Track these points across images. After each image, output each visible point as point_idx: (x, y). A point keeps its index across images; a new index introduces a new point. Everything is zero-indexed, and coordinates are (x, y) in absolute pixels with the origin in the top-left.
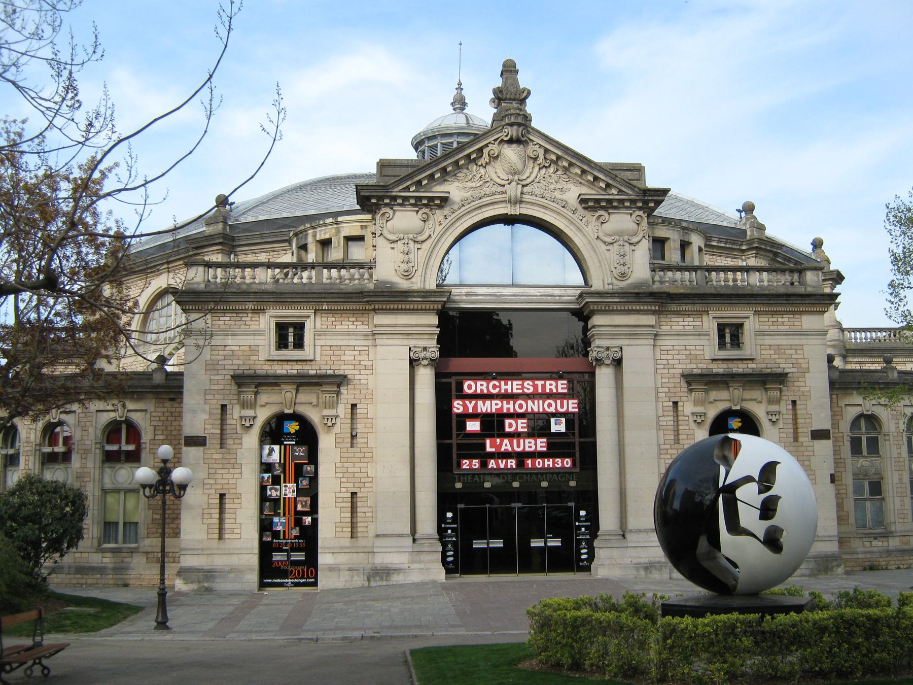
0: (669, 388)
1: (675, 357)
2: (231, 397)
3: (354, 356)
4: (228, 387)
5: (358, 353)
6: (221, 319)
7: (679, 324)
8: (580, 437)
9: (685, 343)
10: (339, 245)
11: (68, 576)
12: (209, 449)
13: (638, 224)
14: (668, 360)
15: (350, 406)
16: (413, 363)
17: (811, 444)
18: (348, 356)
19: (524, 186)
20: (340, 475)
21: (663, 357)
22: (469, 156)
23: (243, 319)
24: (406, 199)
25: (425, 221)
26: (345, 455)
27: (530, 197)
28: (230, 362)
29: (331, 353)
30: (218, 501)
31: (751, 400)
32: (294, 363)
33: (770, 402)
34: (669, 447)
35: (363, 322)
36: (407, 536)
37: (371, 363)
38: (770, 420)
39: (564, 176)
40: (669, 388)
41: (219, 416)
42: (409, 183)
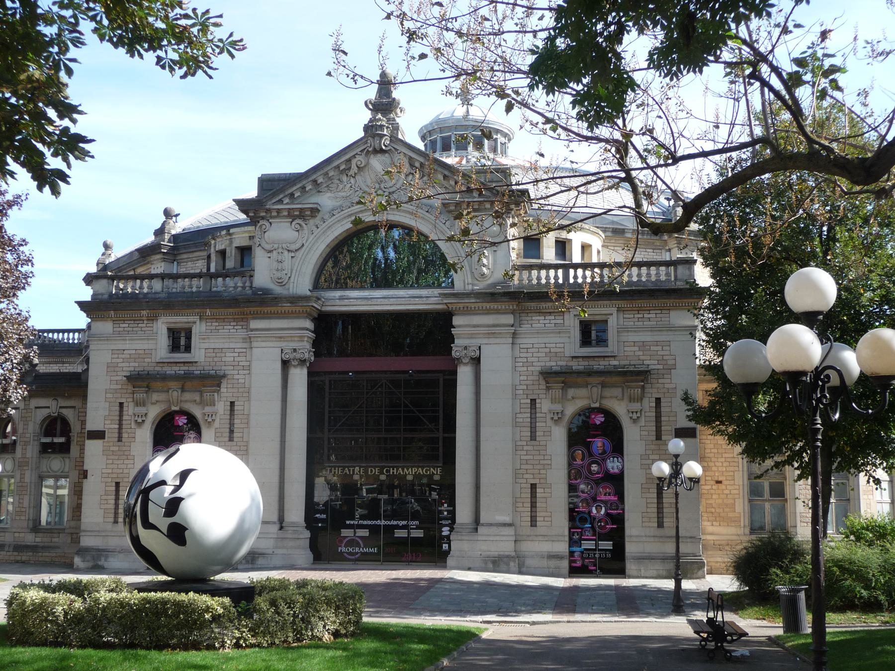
0: (527, 385)
1: (535, 355)
2: (127, 396)
4: (125, 387)
5: (237, 354)
6: (121, 325)
7: (538, 322)
8: (444, 432)
9: (546, 340)
10: (231, 255)
11: (8, 553)
12: (108, 442)
14: (527, 358)
15: (229, 404)
18: (229, 358)
21: (522, 355)
22: (338, 167)
23: (140, 325)
24: (279, 211)
28: (127, 364)
29: (214, 355)
30: (114, 488)
31: (611, 397)
33: (631, 399)
36: (274, 523)
37: (248, 364)
38: (631, 418)
40: (527, 385)
41: (118, 413)
42: (281, 196)
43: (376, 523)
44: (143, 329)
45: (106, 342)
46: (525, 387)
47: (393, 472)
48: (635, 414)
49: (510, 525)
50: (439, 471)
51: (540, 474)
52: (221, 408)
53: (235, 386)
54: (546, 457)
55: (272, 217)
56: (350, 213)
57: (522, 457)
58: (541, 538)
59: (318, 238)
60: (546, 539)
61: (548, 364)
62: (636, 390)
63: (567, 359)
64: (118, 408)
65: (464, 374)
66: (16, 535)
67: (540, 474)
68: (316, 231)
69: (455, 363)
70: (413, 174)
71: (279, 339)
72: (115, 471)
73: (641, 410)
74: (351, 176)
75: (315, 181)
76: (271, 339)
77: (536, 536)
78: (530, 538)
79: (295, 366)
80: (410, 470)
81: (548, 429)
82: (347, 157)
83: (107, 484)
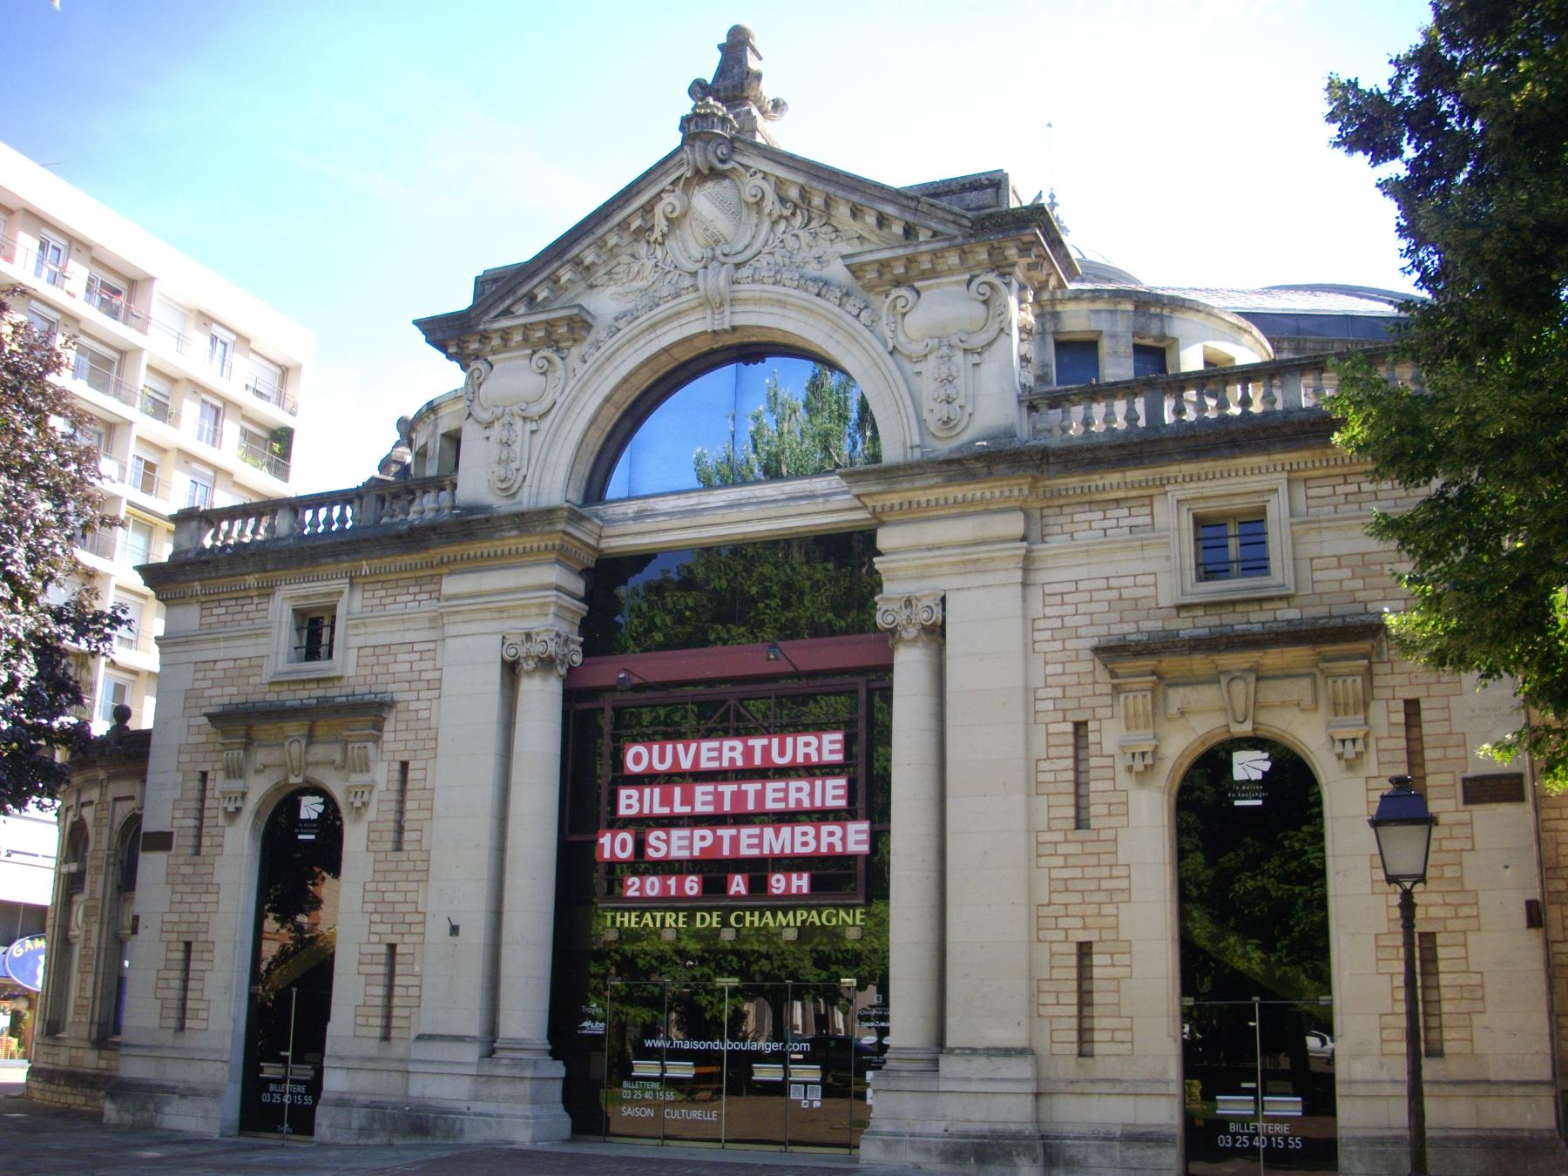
0: (1064, 687)
3: (412, 662)
9: (1108, 570)
12: (177, 855)
13: (985, 302)
16: (511, 670)
17: (1465, 816)
19: (738, 266)
20: (370, 907)
21: (1049, 611)
23: (246, 609)
24: (505, 334)
25: (544, 374)
26: (382, 867)
27: (750, 287)
29: (374, 659)
31: (1284, 704)
32: (314, 686)
34: (1059, 837)
35: (430, 592)
36: (473, 1039)
38: (1340, 756)
39: (823, 230)
40: (1064, 687)
43: (712, 1046)
44: (251, 615)
45: (186, 648)
46: (1058, 692)
47: (752, 922)
48: (1349, 745)
49: (1022, 1052)
50: (858, 917)
51: (1100, 915)
52: (382, 775)
53: (412, 725)
54: (1116, 872)
55: (494, 352)
56: (652, 321)
57: (1055, 874)
58: (1104, 1088)
59: (585, 384)
60: (1118, 1090)
61: (1118, 630)
62: (1349, 681)
63: (1164, 613)
64: (196, 784)
65: (909, 667)
66: (74, 1052)
67: (1100, 915)
68: (581, 370)
69: (889, 638)
70: (786, 218)
71: (496, 615)
72: (185, 917)
73: (1366, 736)
74: (655, 241)
75: (577, 262)
76: (482, 616)
77: (1092, 1081)
78: (1077, 1088)
79: (530, 673)
80: (791, 914)
81: (1121, 797)
82: (643, 199)
83: (171, 946)
